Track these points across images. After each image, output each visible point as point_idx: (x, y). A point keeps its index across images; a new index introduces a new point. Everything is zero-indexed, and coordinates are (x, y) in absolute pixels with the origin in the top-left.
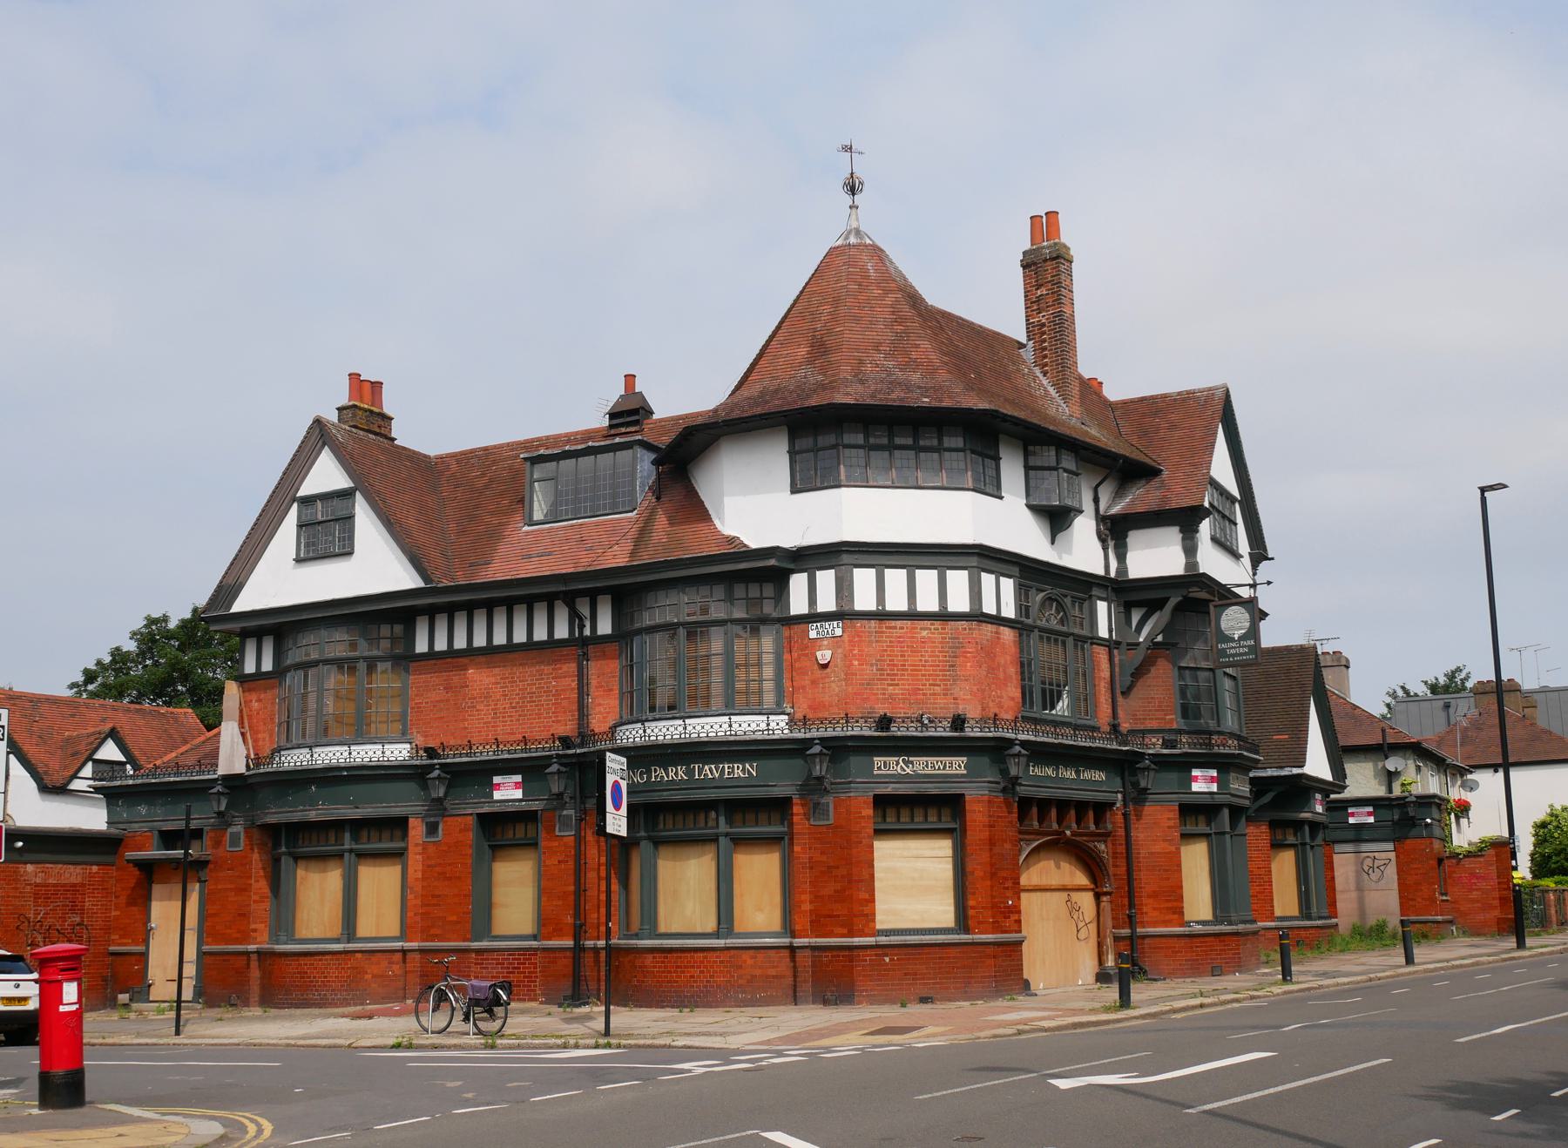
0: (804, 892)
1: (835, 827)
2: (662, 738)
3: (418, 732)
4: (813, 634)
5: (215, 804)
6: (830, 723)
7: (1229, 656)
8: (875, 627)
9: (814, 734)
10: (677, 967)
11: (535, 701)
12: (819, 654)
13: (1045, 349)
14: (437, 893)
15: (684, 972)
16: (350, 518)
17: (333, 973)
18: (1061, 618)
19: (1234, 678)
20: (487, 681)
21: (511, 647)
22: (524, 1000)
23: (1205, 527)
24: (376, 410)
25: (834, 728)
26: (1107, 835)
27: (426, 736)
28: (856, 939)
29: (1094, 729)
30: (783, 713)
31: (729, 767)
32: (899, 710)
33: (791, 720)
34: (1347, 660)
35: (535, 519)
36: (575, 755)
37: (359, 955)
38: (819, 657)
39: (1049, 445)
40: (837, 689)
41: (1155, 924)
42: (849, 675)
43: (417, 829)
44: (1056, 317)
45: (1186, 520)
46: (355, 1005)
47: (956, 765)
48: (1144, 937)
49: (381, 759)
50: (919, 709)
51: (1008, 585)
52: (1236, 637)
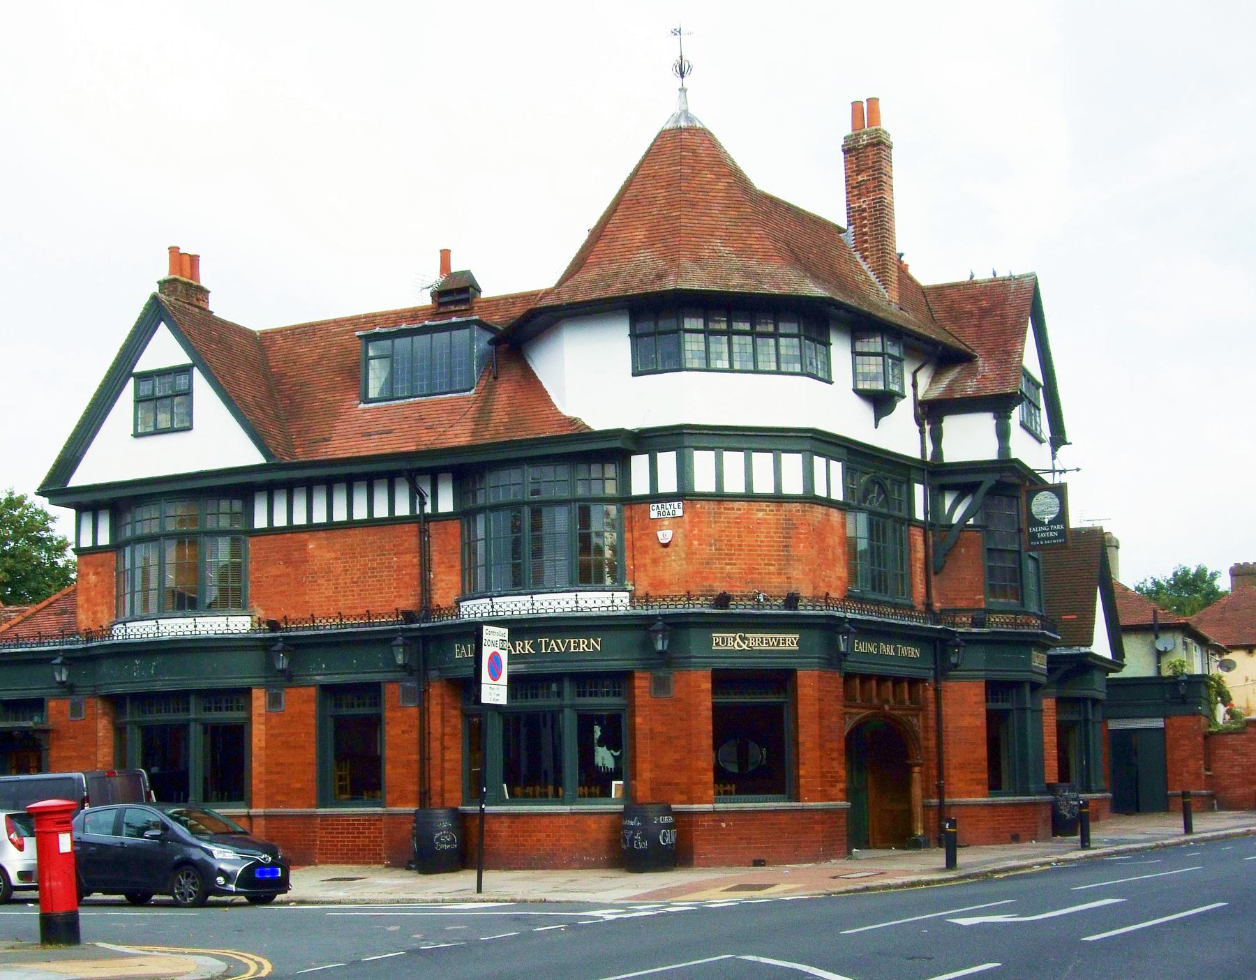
2: (510, 613)
6: (672, 600)
8: (714, 509)
9: (656, 611)
10: (524, 832)
11: (376, 577)
12: (660, 534)
16: (188, 393)
20: (328, 556)
21: (351, 524)
23: (1016, 415)
24: (195, 283)
25: (676, 605)
27: (267, 610)
28: (695, 806)
32: (736, 588)
35: (370, 396)
36: (420, 629)
40: (678, 568)
42: (690, 555)
44: (877, 203)
45: (999, 405)
47: (789, 642)
48: (953, 805)
49: (575, 609)
51: (837, 467)
52: (1046, 521)
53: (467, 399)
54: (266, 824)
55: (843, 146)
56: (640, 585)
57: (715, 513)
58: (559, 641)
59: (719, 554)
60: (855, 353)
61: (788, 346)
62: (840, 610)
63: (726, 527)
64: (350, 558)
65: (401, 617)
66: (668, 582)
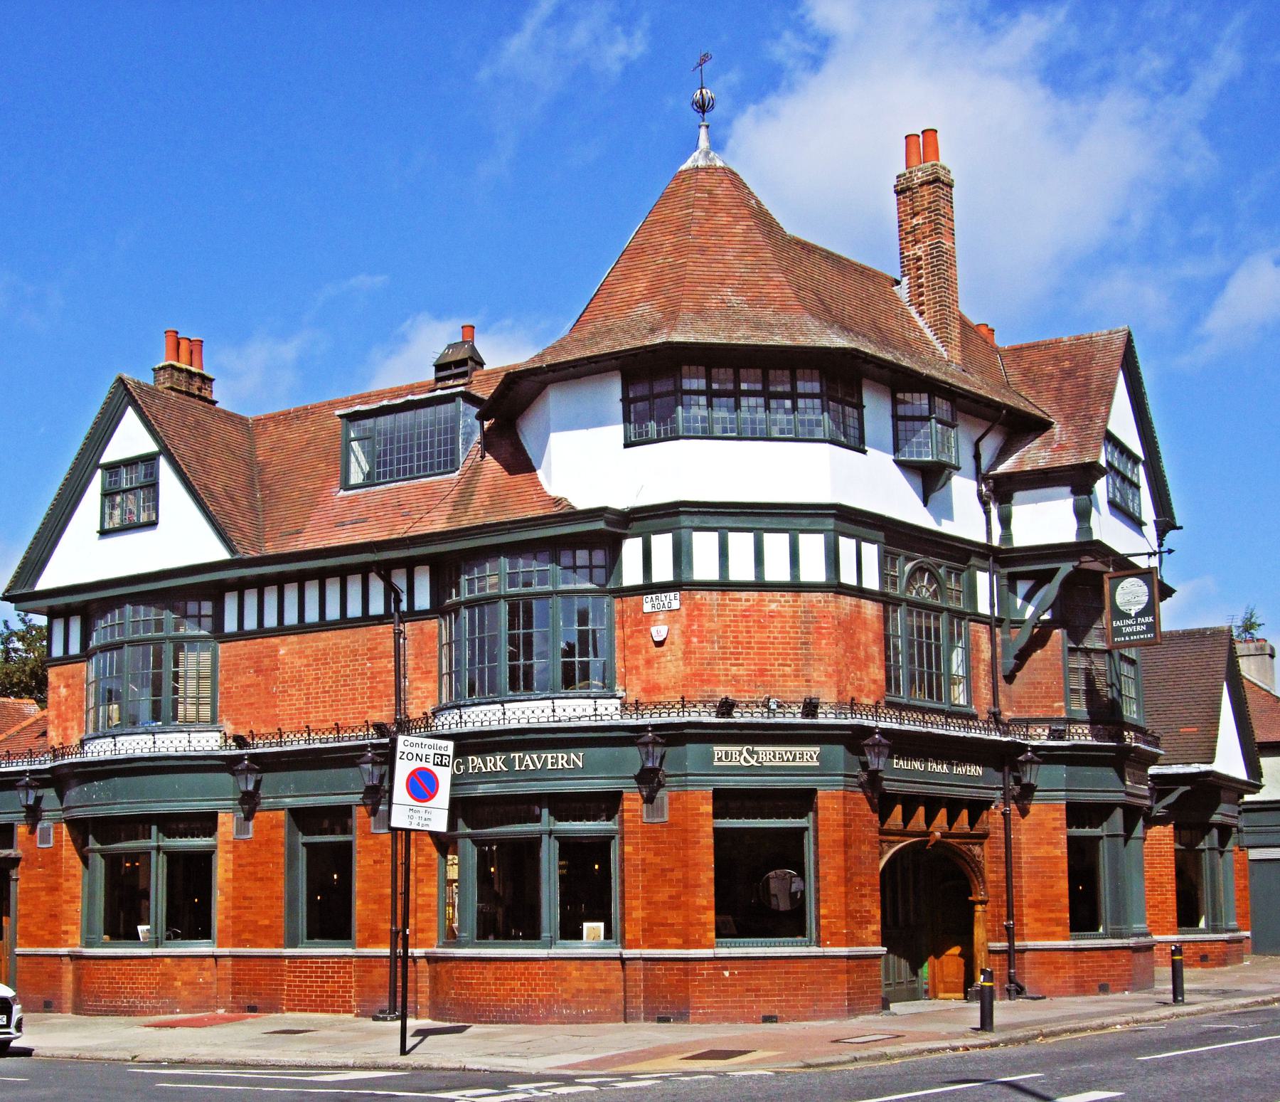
0: (636, 898)
1: (669, 826)
3: (228, 719)
4: (647, 608)
5: (22, 795)
6: (664, 708)
7: (1124, 635)
9: (646, 720)
12: (653, 630)
13: (921, 286)
14: (249, 895)
15: (503, 985)
16: (152, 487)
17: (142, 979)
18: (935, 590)
19: (1132, 662)
22: (339, 1012)
23: (1101, 488)
26: (985, 836)
27: (236, 724)
29: (974, 717)
30: (614, 697)
31: (552, 758)
32: (743, 694)
33: (623, 705)
34: (1272, 649)
37: (168, 961)
38: (654, 634)
39: (920, 392)
40: (673, 670)
41: (1035, 937)
42: (687, 654)
43: (227, 823)
46: (165, 1013)
47: (808, 755)
48: (1023, 951)
50: (766, 692)
51: (871, 552)
53: (450, 482)
54: (232, 965)
55: (895, 186)
56: (632, 690)
57: (718, 605)
58: (535, 756)
59: (723, 653)
60: (896, 418)
61: (811, 410)
62: (870, 717)
63: (731, 621)
64: (322, 664)
65: (372, 730)
66: (662, 686)
